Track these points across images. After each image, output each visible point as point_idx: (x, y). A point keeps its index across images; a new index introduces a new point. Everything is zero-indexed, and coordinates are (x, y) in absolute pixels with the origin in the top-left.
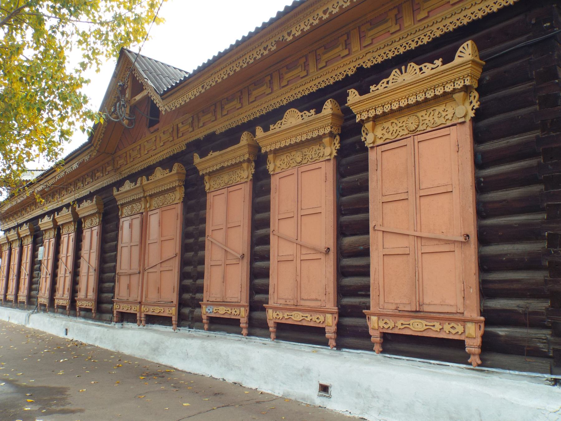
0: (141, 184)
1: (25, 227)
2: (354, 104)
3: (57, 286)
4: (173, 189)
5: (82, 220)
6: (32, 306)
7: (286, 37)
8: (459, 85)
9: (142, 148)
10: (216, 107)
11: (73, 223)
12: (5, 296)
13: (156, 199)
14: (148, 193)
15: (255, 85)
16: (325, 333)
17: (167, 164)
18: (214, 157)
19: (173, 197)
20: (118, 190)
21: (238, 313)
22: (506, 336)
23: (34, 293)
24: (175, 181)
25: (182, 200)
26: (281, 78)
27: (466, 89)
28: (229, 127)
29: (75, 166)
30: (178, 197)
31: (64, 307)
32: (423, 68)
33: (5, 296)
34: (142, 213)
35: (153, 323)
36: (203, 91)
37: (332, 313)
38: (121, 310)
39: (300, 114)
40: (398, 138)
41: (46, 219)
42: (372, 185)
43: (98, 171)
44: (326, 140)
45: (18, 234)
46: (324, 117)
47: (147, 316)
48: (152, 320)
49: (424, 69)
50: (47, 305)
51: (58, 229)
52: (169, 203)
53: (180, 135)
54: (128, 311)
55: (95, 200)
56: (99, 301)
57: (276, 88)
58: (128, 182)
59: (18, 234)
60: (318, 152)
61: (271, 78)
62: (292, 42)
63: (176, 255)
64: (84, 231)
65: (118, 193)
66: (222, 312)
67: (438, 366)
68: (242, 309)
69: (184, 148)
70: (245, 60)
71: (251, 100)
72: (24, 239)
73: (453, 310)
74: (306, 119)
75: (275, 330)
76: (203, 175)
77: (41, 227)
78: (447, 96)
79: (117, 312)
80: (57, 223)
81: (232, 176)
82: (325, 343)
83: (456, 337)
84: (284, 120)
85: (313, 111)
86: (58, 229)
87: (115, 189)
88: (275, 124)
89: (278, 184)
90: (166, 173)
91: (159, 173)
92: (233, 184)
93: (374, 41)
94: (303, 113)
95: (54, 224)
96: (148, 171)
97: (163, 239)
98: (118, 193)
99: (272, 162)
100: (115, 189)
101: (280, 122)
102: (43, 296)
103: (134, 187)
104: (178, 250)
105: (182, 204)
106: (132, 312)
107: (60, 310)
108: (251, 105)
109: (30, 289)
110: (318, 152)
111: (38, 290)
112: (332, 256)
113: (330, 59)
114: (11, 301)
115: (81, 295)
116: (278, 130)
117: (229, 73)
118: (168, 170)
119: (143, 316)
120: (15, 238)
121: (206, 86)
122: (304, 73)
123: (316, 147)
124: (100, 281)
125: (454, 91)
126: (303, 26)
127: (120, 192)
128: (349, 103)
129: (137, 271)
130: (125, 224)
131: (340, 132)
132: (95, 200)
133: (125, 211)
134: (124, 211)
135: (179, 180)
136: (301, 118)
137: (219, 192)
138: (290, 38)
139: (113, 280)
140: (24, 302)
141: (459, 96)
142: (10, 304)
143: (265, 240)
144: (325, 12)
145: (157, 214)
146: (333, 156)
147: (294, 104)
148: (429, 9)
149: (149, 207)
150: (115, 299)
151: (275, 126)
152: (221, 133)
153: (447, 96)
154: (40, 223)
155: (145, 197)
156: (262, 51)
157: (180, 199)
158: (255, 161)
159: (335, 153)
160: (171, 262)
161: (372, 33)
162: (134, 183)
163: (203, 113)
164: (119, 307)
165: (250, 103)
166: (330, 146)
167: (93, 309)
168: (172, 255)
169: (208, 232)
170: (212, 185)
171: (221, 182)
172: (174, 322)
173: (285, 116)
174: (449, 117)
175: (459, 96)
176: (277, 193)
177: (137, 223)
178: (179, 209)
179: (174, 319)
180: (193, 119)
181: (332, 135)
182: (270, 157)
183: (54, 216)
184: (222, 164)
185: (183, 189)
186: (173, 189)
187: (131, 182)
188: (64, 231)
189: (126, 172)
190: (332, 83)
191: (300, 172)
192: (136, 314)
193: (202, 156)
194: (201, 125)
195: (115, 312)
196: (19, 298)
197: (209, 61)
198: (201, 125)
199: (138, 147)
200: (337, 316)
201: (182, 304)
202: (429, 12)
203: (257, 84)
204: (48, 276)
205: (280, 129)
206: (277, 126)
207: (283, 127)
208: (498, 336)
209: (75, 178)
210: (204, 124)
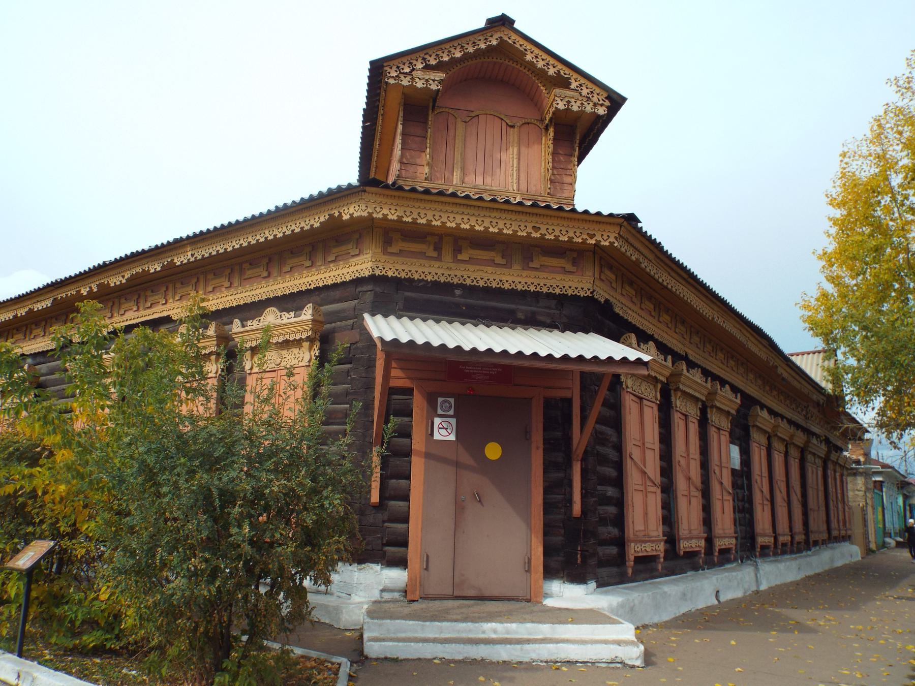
8: (304, 336)
11: (213, 357)
28: (357, 275)
29: (48, 303)
32: (283, 316)
36: (192, 259)
39: (279, 314)
44: (306, 345)
46: (302, 321)
49: (283, 317)
60: (298, 356)
61: (360, 237)
67: (509, 594)
81: (286, 356)
84: (263, 317)
87: (237, 322)
93: (126, 313)
94: (282, 313)
99: (249, 359)
101: (258, 319)
110: (298, 356)
123: (296, 351)
148: (336, 254)
161: (214, 282)
163: (337, 241)
173: (264, 314)
174: (300, 359)
181: (310, 339)
184: (287, 337)
202: (291, 268)
203: (253, 264)
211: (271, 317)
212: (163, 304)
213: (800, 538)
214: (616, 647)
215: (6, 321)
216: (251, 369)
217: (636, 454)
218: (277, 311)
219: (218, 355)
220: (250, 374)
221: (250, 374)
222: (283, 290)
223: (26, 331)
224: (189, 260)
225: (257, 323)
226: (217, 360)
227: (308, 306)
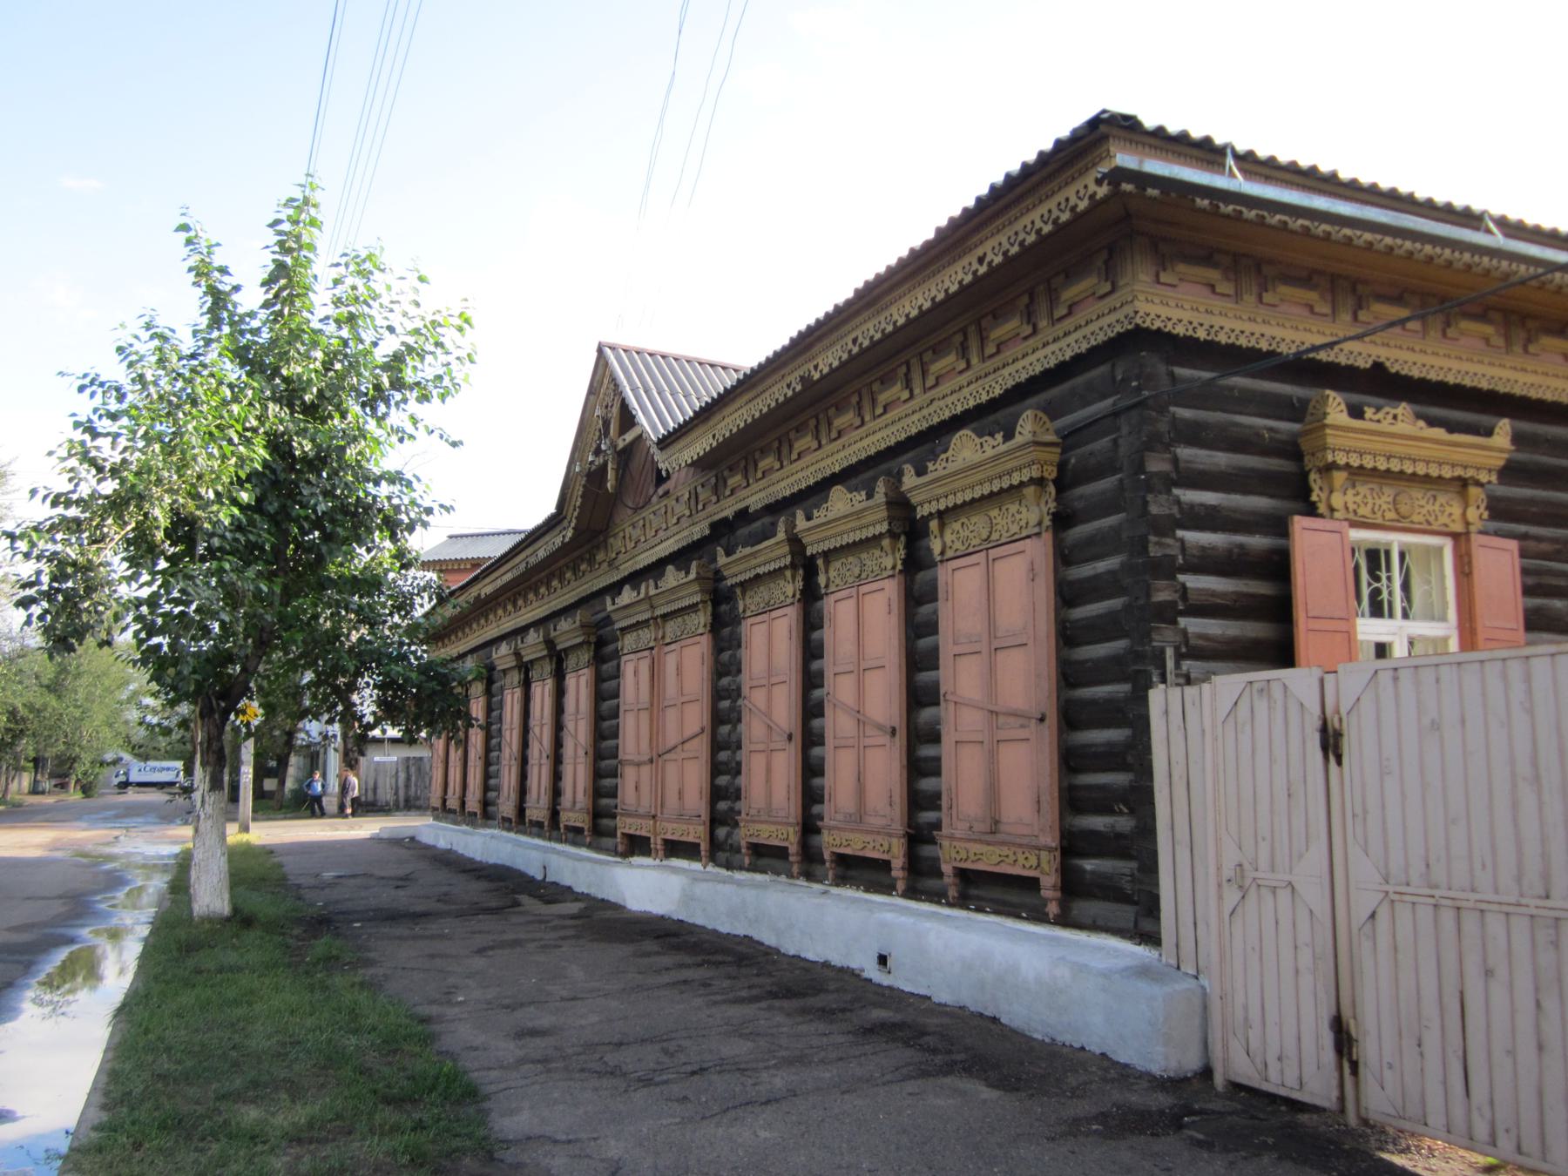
0: (647, 593)
1: (533, 637)
2: (910, 490)
3: (528, 782)
4: (693, 608)
5: (820, 562)
6: (490, 822)
7: (813, 372)
9: (647, 525)
10: (966, 338)
11: (788, 573)
12: (444, 801)
13: (672, 623)
14: (659, 612)
15: (797, 431)
16: (1039, 890)
17: (680, 558)
18: (745, 557)
19: (696, 622)
20: (809, 518)
21: (886, 847)
22: (1093, 872)
23: (492, 795)
24: (880, 522)
25: (708, 628)
26: (1053, 301)
27: (1040, 482)
30: (702, 622)
31: (539, 825)
33: (444, 801)
34: (652, 648)
35: (677, 856)
36: (983, 270)
37: (1050, 850)
38: (669, 837)
39: (978, 441)
40: (971, 550)
41: (504, 649)
42: (943, 625)
43: (582, 560)
44: (886, 542)
45: (517, 655)
47: (666, 841)
48: (674, 849)
49: (986, 447)
50: (546, 824)
51: (525, 668)
52: (1005, 535)
53: (700, 507)
54: (682, 839)
55: (578, 618)
56: (597, 814)
57: (1043, 324)
58: (670, 568)
59: (517, 655)
60: (1018, 517)
62: (819, 381)
63: (703, 730)
64: (568, 677)
65: (811, 524)
66: (988, 860)
68: (791, 830)
69: (707, 532)
70: (967, 267)
71: (1057, 314)
72: (567, 656)
73: (1026, 831)
74: (990, 452)
75: (799, 858)
76: (926, 519)
77: (914, 501)
78: (1014, 491)
79: (623, 834)
80: (804, 548)
81: (999, 519)
82: (887, 889)
83: (776, 843)
85: (999, 437)
86: (525, 668)
87: (608, 600)
88: (936, 461)
89: (950, 581)
90: (994, 445)
91: (672, 577)
92: (1003, 540)
94: (983, 440)
95: (792, 553)
96: (655, 569)
97: (996, 644)
98: (811, 524)
100: (608, 600)
102: (506, 805)
103: (864, 504)
104: (706, 720)
105: (902, 578)
106: (690, 839)
107: (535, 830)
108: (1058, 326)
109: (486, 788)
111: (497, 789)
112: (901, 740)
113: (1077, 299)
114: (454, 812)
115: (566, 800)
116: (941, 473)
117: (1041, 229)
118: (999, 437)
119: (659, 842)
120: (539, 655)
121: (860, 340)
122: (1107, 287)
124: (597, 775)
125: (1022, 484)
126: (947, 283)
127: (660, 590)
128: (904, 488)
129: (646, 758)
130: (628, 669)
131: (907, 529)
132: (578, 618)
133: (835, 574)
134: (626, 642)
135: (702, 591)
136: (980, 451)
137: (759, 618)
138: (816, 376)
139: (614, 774)
140: (475, 814)
141: (1030, 491)
142: (452, 816)
143: (734, 718)
144: (981, 260)
145: (977, 568)
146: (1044, 528)
147: (842, 477)
149: (663, 637)
150: (619, 810)
151: (937, 465)
152: (756, 511)
153: (1014, 491)
154: (494, 656)
155: (655, 619)
156: (786, 390)
157: (705, 626)
158: (906, 534)
159: (899, 567)
160: (696, 741)
162: (863, 493)
164: (626, 825)
165: (1055, 322)
166: (1038, 505)
167: (586, 828)
168: (697, 729)
169: (745, 691)
170: (949, 543)
171: (971, 536)
172: (703, 853)
174: (1023, 523)
175: (1030, 491)
176: (950, 602)
177: (644, 667)
178: (1040, 551)
179: (704, 847)
180: (818, 422)
182: (934, 525)
183: (791, 525)
185: (710, 608)
186: (693, 608)
187: (679, 569)
188: (571, 662)
189: (626, 569)
190: (1067, 358)
191: (990, 558)
192: (699, 845)
193: (728, 554)
194: (794, 456)
195: (619, 834)
196: (528, 812)
197: (878, 276)
198: (794, 456)
199: (641, 523)
200: (1058, 854)
201: (715, 820)
204: (513, 762)
205: (946, 472)
206: (822, 512)
207: (952, 467)
208: (1084, 871)
209: (547, 572)
210: (840, 434)
211: (966, 449)
212: (905, 401)
213: (473, 804)
214: (1174, 940)
215: (754, 420)
216: (942, 553)
217: (544, 761)
218: (974, 436)
219: (892, 534)
220: (941, 561)
221: (941, 561)
222: (1031, 368)
223: (817, 427)
224: (975, 273)
225: (944, 464)
226: (705, 608)
227: (1024, 416)
